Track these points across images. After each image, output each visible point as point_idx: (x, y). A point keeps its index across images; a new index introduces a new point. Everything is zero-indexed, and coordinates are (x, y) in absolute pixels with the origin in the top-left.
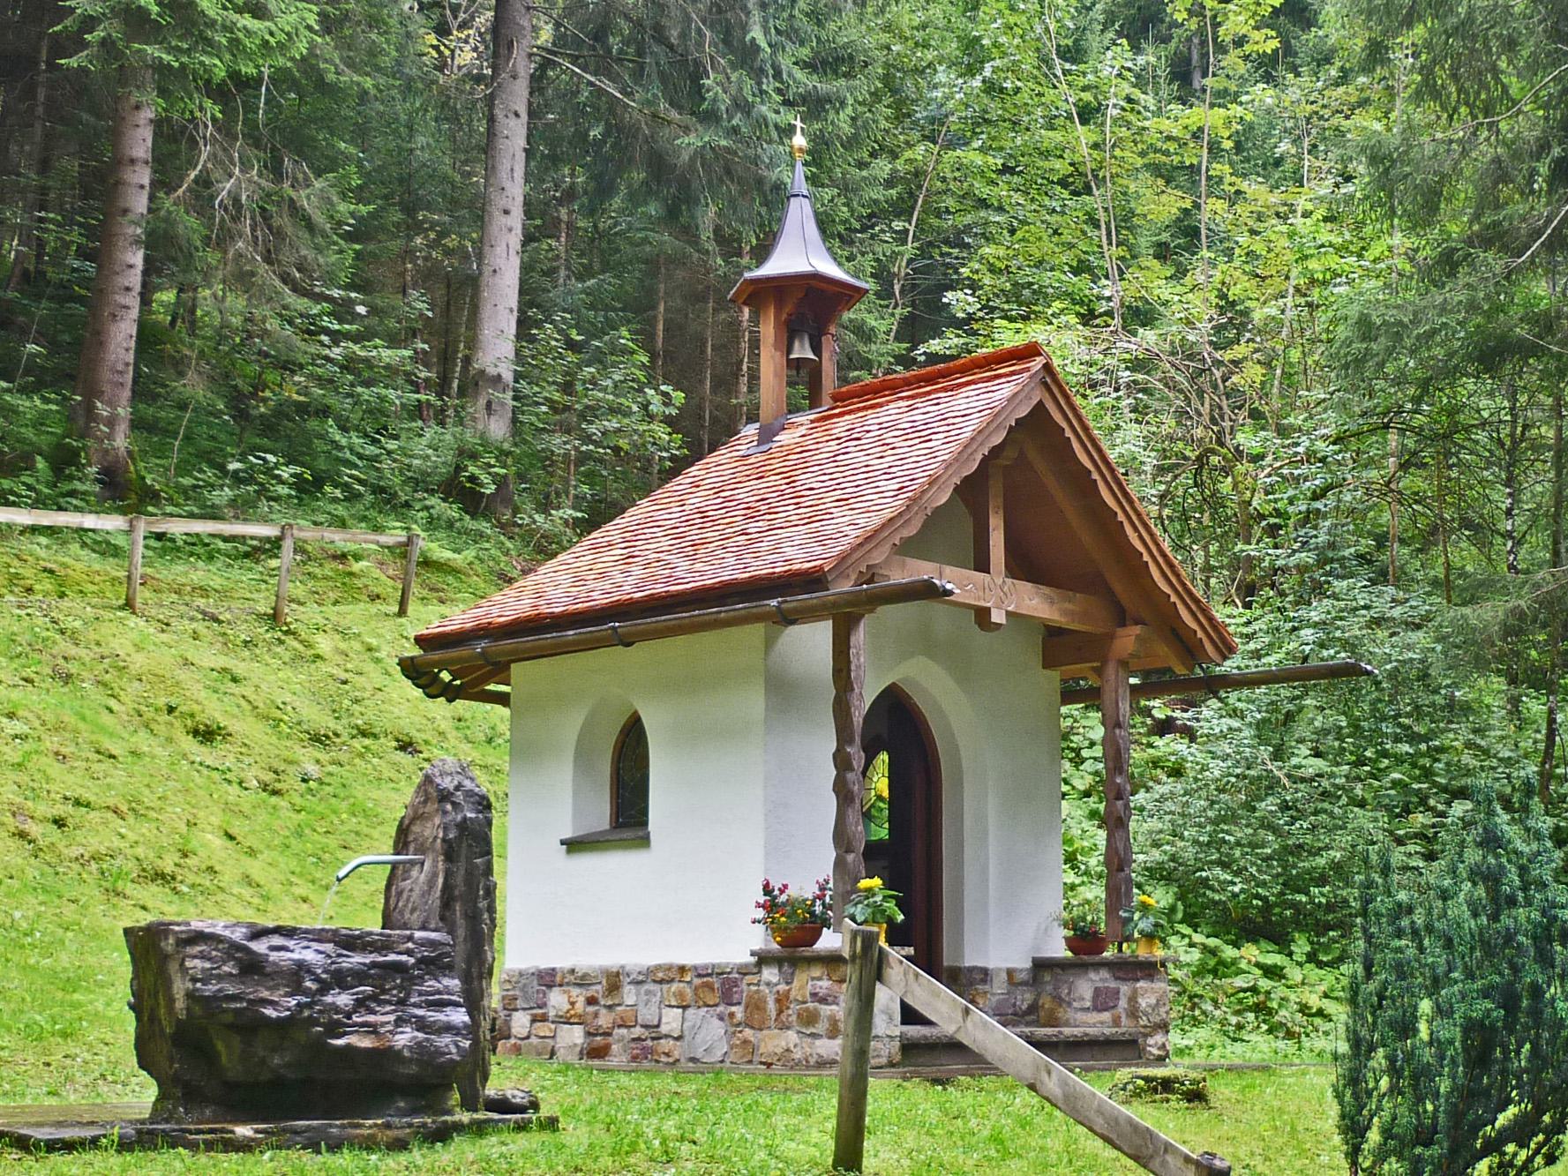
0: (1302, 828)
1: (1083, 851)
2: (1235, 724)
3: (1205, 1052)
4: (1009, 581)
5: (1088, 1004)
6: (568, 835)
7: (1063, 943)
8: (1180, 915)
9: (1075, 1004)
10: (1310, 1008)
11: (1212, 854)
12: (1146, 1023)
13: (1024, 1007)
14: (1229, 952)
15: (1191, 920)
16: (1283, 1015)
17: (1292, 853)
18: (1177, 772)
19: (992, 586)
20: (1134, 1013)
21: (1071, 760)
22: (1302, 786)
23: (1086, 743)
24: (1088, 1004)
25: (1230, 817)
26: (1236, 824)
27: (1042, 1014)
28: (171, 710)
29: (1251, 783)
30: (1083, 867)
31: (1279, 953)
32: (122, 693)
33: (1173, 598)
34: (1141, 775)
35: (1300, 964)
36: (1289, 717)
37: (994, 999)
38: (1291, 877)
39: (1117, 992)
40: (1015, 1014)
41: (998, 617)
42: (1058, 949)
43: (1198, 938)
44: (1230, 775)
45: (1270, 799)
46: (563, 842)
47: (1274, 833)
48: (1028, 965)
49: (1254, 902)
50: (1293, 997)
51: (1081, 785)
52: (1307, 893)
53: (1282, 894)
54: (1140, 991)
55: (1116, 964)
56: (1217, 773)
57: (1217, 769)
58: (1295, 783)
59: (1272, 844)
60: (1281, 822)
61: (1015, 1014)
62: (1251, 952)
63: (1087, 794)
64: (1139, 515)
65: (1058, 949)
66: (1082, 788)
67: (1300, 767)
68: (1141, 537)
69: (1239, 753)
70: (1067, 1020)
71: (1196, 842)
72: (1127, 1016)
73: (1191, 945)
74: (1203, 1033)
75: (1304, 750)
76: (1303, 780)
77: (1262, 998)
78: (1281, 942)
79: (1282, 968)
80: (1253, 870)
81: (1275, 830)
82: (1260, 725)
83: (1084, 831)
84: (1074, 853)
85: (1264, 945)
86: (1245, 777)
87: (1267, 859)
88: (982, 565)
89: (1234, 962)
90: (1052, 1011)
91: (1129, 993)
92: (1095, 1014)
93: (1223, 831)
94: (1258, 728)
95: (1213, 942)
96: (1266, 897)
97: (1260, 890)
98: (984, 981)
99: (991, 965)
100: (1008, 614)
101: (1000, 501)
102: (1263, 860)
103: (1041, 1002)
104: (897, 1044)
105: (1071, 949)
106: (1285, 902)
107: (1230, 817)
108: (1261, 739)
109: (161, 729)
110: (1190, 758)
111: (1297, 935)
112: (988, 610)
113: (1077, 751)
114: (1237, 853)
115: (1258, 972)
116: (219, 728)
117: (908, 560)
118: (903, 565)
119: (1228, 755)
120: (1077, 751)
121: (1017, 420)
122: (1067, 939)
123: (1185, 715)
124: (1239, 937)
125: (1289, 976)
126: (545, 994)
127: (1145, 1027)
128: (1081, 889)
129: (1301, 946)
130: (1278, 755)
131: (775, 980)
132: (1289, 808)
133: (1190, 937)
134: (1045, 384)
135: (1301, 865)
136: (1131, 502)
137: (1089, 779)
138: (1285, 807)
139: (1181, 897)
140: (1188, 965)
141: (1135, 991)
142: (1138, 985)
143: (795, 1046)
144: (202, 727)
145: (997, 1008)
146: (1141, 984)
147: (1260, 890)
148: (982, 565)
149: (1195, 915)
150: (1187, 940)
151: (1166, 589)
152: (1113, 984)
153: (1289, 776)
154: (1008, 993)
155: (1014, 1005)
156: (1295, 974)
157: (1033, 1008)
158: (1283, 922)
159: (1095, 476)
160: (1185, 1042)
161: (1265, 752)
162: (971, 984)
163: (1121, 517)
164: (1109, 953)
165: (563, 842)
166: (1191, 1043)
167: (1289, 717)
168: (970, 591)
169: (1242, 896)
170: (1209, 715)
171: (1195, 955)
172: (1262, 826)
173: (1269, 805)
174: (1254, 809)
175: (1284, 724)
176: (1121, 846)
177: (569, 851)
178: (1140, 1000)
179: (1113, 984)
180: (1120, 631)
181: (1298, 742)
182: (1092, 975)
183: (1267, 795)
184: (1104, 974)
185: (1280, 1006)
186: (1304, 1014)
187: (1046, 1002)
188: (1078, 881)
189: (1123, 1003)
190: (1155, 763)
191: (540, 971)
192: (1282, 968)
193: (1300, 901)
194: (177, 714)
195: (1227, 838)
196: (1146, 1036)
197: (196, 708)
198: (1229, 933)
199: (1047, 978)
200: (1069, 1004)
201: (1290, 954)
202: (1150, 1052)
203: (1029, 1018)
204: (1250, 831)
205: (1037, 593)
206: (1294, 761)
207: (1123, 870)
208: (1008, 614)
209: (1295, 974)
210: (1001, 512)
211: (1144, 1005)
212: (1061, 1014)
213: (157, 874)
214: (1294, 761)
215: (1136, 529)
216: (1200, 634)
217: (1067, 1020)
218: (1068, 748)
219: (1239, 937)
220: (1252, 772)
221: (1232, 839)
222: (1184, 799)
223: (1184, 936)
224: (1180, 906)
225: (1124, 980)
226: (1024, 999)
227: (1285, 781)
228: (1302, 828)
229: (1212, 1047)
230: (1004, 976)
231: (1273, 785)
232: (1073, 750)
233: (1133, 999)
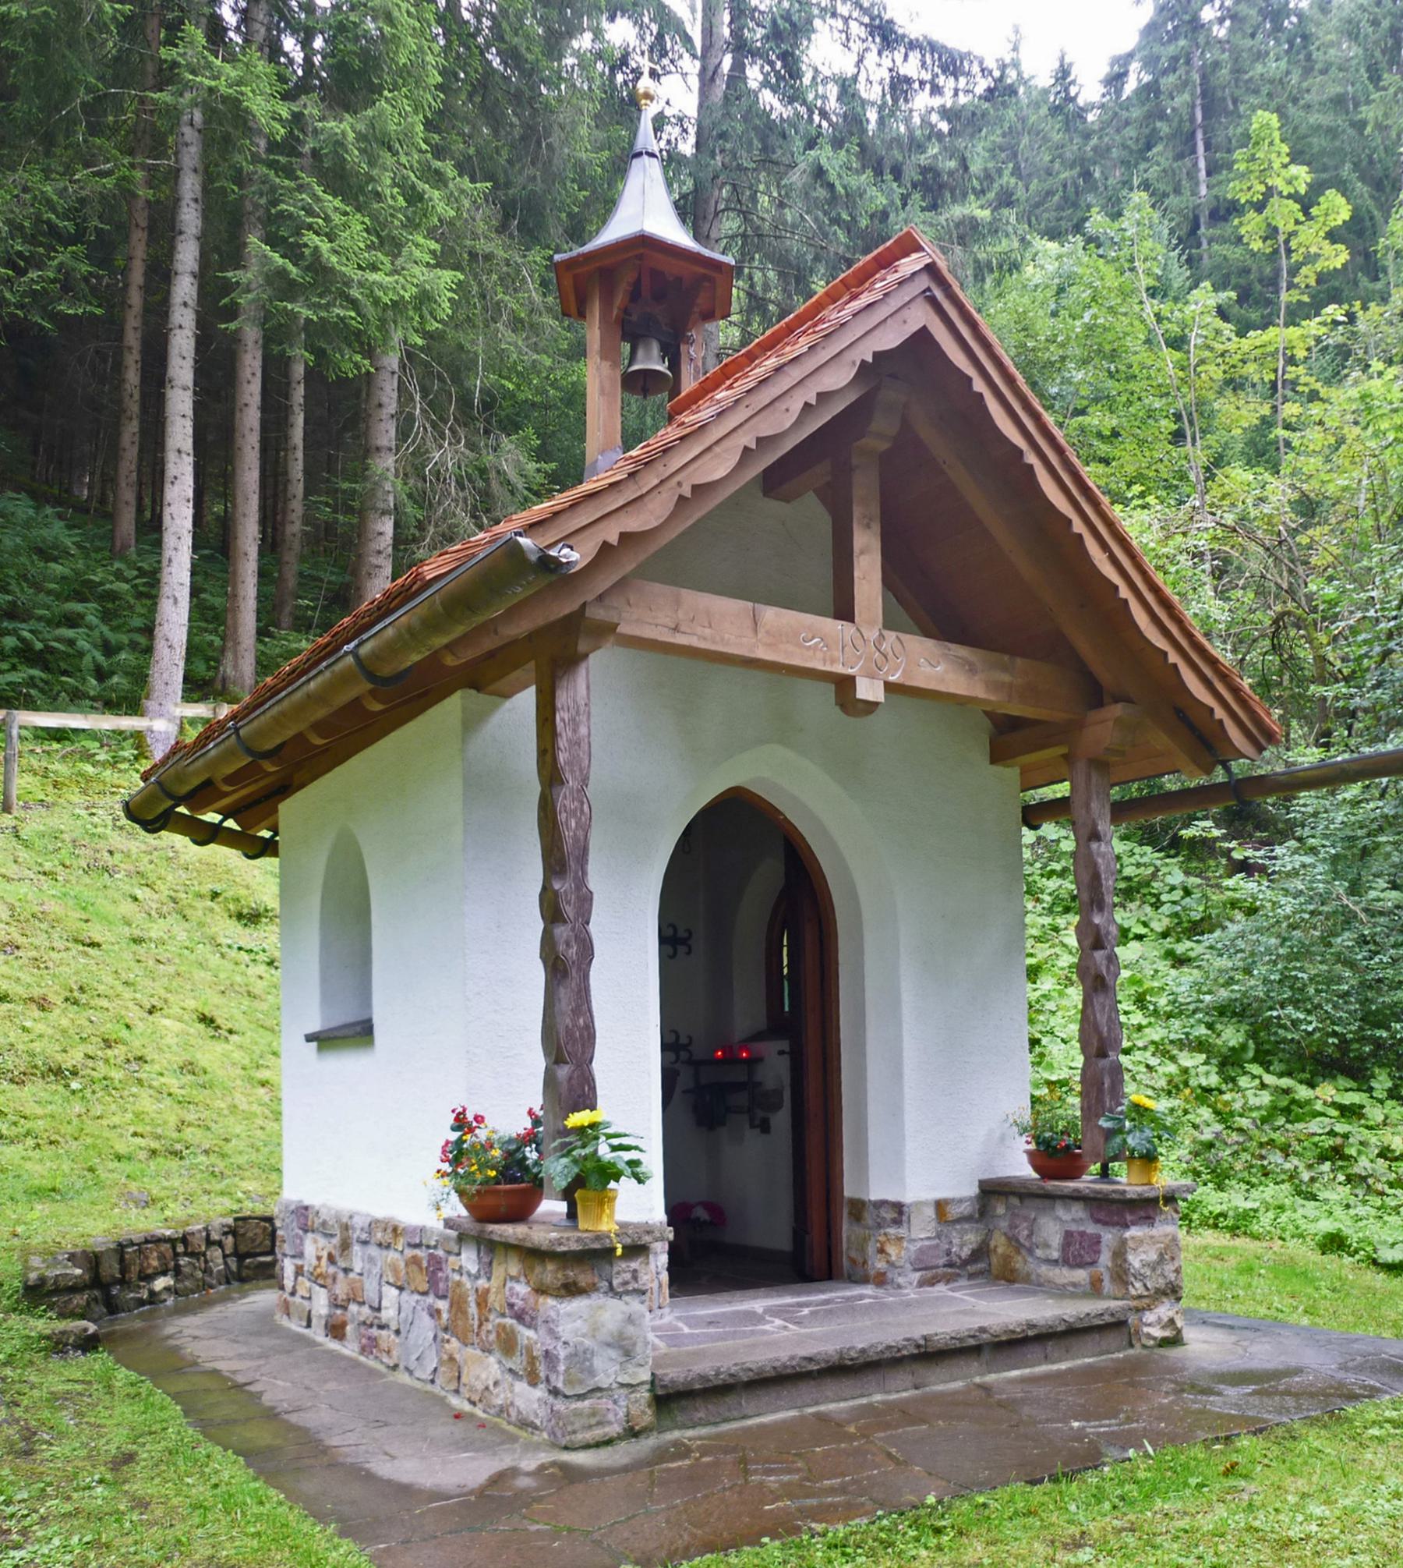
0: (1381, 962)
1: (1150, 991)
2: (1308, 860)
3: (1271, 1215)
4: (891, 636)
5: (1055, 1255)
6: (315, 1026)
7: (1025, 1158)
8: (1251, 1054)
9: (1039, 1253)
10: (1393, 1151)
11: (1284, 992)
12: (1141, 1291)
13: (965, 1252)
14: (1303, 1092)
15: (1263, 1058)
16: (1363, 1165)
17: (1370, 987)
18: (1251, 911)
19: (859, 642)
20: (1121, 1275)
21: (1152, 905)
22: (1382, 920)
23: (1167, 888)
24: (1055, 1255)
25: (1302, 953)
26: (1311, 962)
27: (994, 1260)
28: (215, 895)
29: (1327, 919)
30: (1151, 1008)
31: (1359, 1090)
32: (159, 882)
33: (1173, 657)
34: (1218, 916)
35: (1381, 1102)
36: (1365, 852)
37: (913, 1248)
38: (1370, 1013)
39: (1096, 1241)
40: (950, 1265)
41: (868, 690)
42: (1019, 1166)
43: (1269, 1079)
44: (1303, 911)
45: (1347, 934)
46: (309, 1038)
47: (1351, 968)
48: (973, 1190)
49: (1330, 1041)
50: (1374, 1140)
51: (1158, 926)
52: (1388, 1028)
53: (1361, 1029)
54: (1131, 1244)
55: (1095, 1199)
56: (1288, 910)
57: (1288, 906)
58: (1373, 916)
59: (1349, 980)
60: (1359, 957)
61: (950, 1265)
62: (1327, 1091)
63: (1165, 935)
64: (1110, 524)
65: (1019, 1166)
66: (1159, 930)
67: (1379, 900)
68: (1114, 560)
69: (1312, 889)
70: (1028, 1275)
71: (1266, 981)
72: (1113, 1279)
73: (1263, 1086)
74: (1270, 1192)
75: (1382, 883)
76: (1382, 913)
77: (1339, 1141)
78: (1358, 1073)
79: (1362, 1107)
80: (1329, 1008)
81: (1351, 964)
82: (1335, 859)
83: (1156, 971)
84: (1144, 993)
85: (1343, 1082)
86: (1320, 913)
87: (1345, 995)
88: (844, 611)
89: (1308, 1102)
90: (1007, 1259)
91: (1114, 1244)
92: (1065, 1271)
93: (1295, 968)
94: (1332, 864)
95: (1286, 1082)
96: (1344, 1035)
97: (1336, 1028)
98: (897, 1222)
99: (908, 1198)
100: (889, 687)
101: (875, 509)
102: (1339, 996)
103: (992, 1244)
104: (644, 1394)
105: (1036, 1169)
106: (1364, 1038)
107: (1302, 953)
108: (1336, 875)
109: (196, 915)
110: (1261, 896)
111: (1377, 1070)
112: (851, 680)
113: (1157, 896)
114: (1311, 991)
115: (1335, 1113)
116: (267, 911)
117: (684, 592)
118: (678, 602)
119: (1301, 891)
120: (1157, 896)
121: (876, 355)
122: (1029, 1153)
123: (1258, 854)
124: (1314, 1074)
125: (1369, 1116)
126: (302, 1240)
127: (1140, 1297)
128: (1147, 1031)
129: (1382, 1082)
130: (1355, 889)
131: (474, 1269)
132: (1367, 943)
133: (1260, 1077)
134: (933, 302)
135: (1381, 1000)
136: (1096, 504)
137: (1166, 921)
138: (1363, 941)
139: (1253, 1035)
140: (1259, 1108)
141: (1123, 1242)
142: (1128, 1234)
143: (496, 1384)
144: (245, 911)
145: (918, 1259)
146: (1134, 1232)
147: (1336, 1028)
148: (844, 611)
149: (1268, 1052)
150: (1257, 1081)
151: (1160, 643)
152: (1091, 1229)
153: (1366, 910)
154: (938, 1236)
155: (948, 1253)
156: (1375, 1114)
157: (981, 1253)
158: (1362, 1059)
159: (1031, 458)
160: (1249, 1205)
161: (1340, 887)
162: (879, 1226)
163: (1078, 526)
164: (1088, 1181)
165: (309, 1038)
166: (1256, 1205)
167: (1365, 852)
168: (815, 648)
169: (1317, 1035)
170: (1285, 856)
171: (1266, 1098)
172: (1338, 961)
173: (1345, 940)
174: (1329, 945)
175: (1362, 859)
176: (1101, 1019)
177: (320, 1049)
178: (1130, 1258)
179: (1091, 1229)
180: (1094, 715)
181: (1375, 876)
182: (1060, 1212)
183: (1343, 930)
184: (1078, 1211)
185: (1359, 1152)
186: (1386, 1159)
187: (999, 1243)
188: (1144, 1022)
189: (1105, 1259)
190: (1234, 904)
191: (92, 1260)
192: (1362, 1107)
193: (1381, 1037)
194: (220, 899)
195: (1300, 975)
196: (1139, 1310)
197: (243, 892)
198: (1304, 1071)
199: (1001, 1210)
200: (1030, 1251)
201: (1370, 1090)
202: (1149, 1336)
203: (971, 1268)
204: (1325, 967)
205: (945, 656)
206: (1372, 894)
207: (1104, 1055)
208: (889, 687)
209: (1375, 1114)
210: (876, 527)
211: (1137, 1264)
212: (1018, 1263)
213: (50, 1070)
214: (1372, 894)
215: (1104, 546)
216: (1220, 713)
217: (1028, 1275)
218: (1150, 894)
219: (1314, 1074)
220: (1325, 908)
221: (1305, 976)
222: (1255, 937)
223: (1254, 1077)
224: (1251, 1044)
225: (1106, 1224)
226: (965, 1241)
227: (1363, 916)
228: (1381, 962)
229: (1281, 1208)
230: (930, 1212)
231: (1348, 919)
232: (1154, 895)
233: (1120, 1254)
